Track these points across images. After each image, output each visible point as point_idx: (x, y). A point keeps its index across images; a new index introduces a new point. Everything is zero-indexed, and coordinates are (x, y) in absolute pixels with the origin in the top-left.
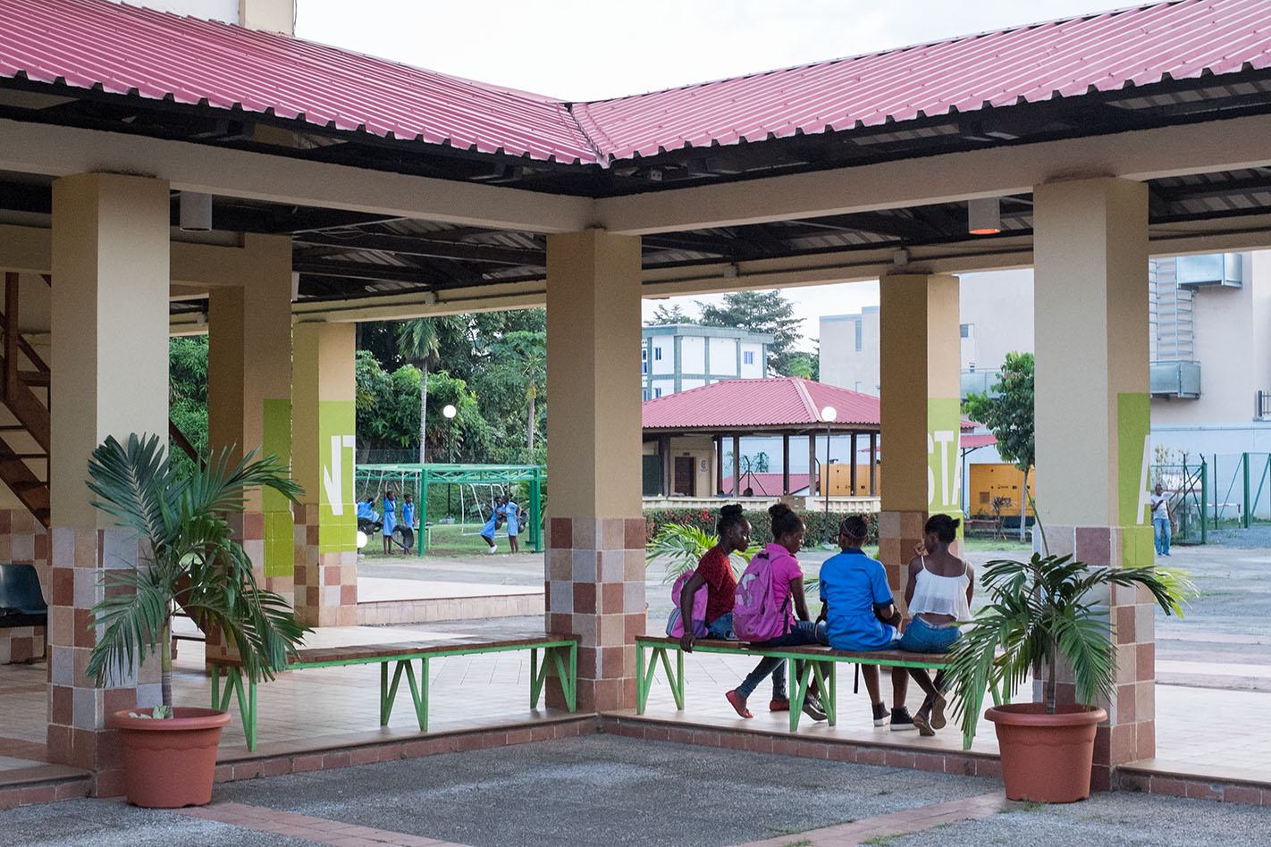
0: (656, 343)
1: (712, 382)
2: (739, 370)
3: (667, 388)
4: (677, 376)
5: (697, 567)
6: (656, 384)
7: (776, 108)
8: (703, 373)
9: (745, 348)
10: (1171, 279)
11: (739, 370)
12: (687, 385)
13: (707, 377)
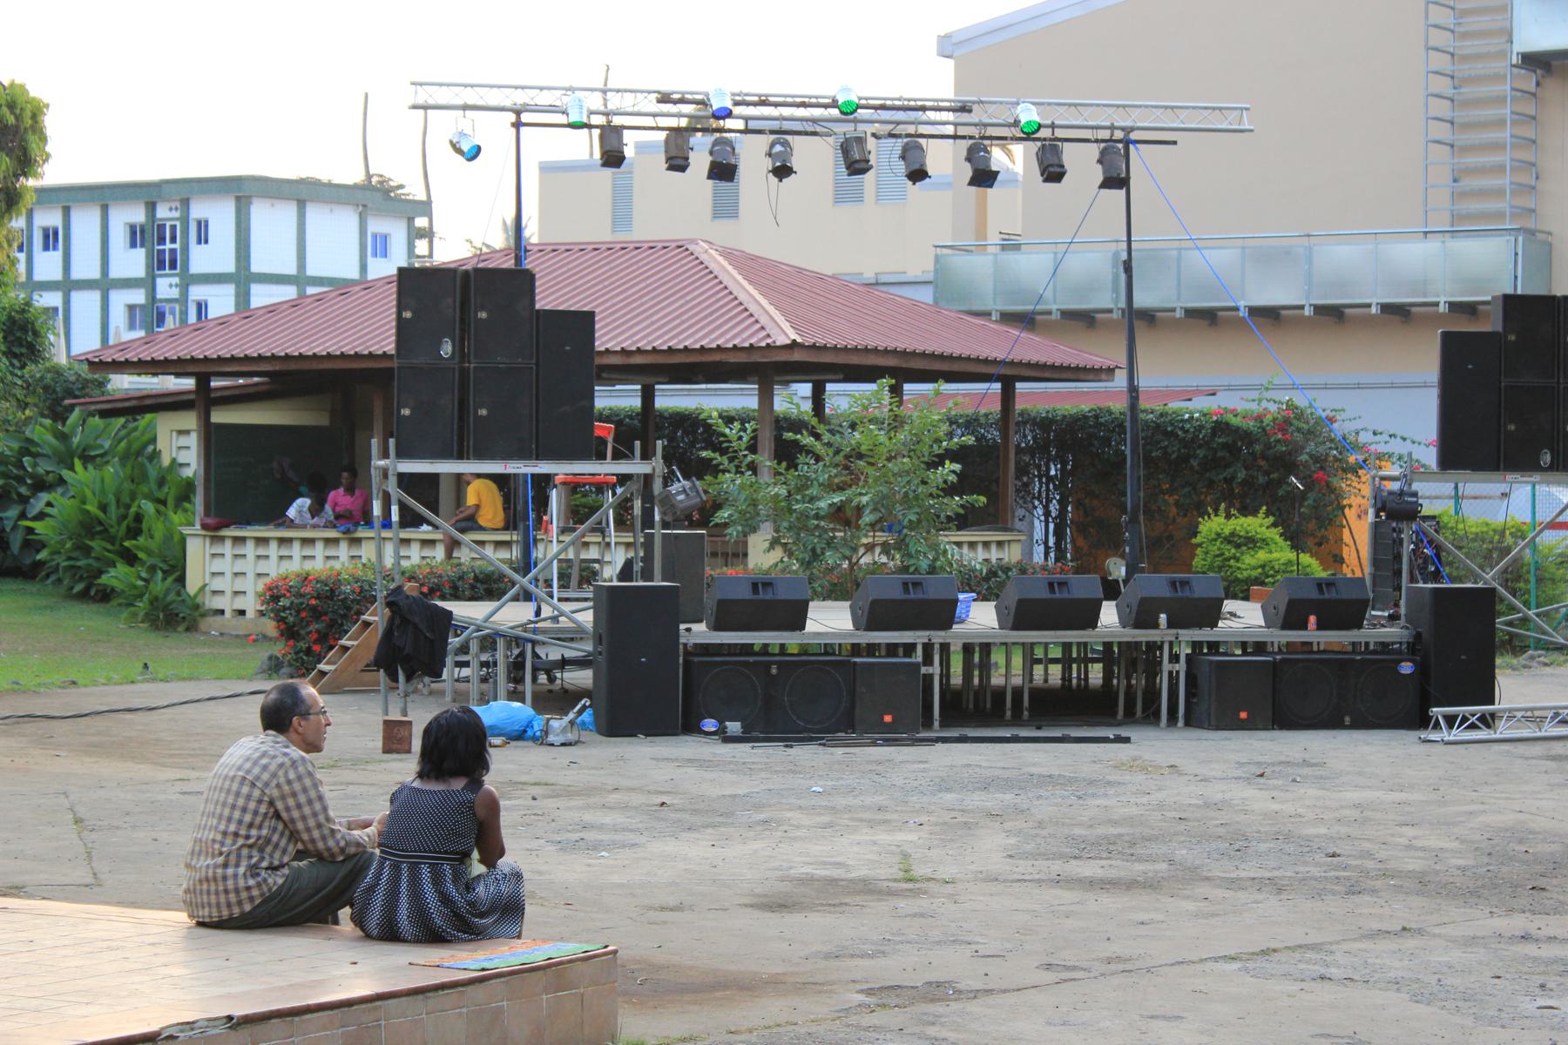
0: (198, 211)
1: (311, 290)
2: (363, 268)
3: (221, 302)
4: (243, 278)
5: (332, 494)
6: (197, 292)
7: (659, 299)
8: (291, 270)
9: (376, 226)
10: (1495, 44)
11: (363, 268)
12: (262, 296)
13: (299, 279)
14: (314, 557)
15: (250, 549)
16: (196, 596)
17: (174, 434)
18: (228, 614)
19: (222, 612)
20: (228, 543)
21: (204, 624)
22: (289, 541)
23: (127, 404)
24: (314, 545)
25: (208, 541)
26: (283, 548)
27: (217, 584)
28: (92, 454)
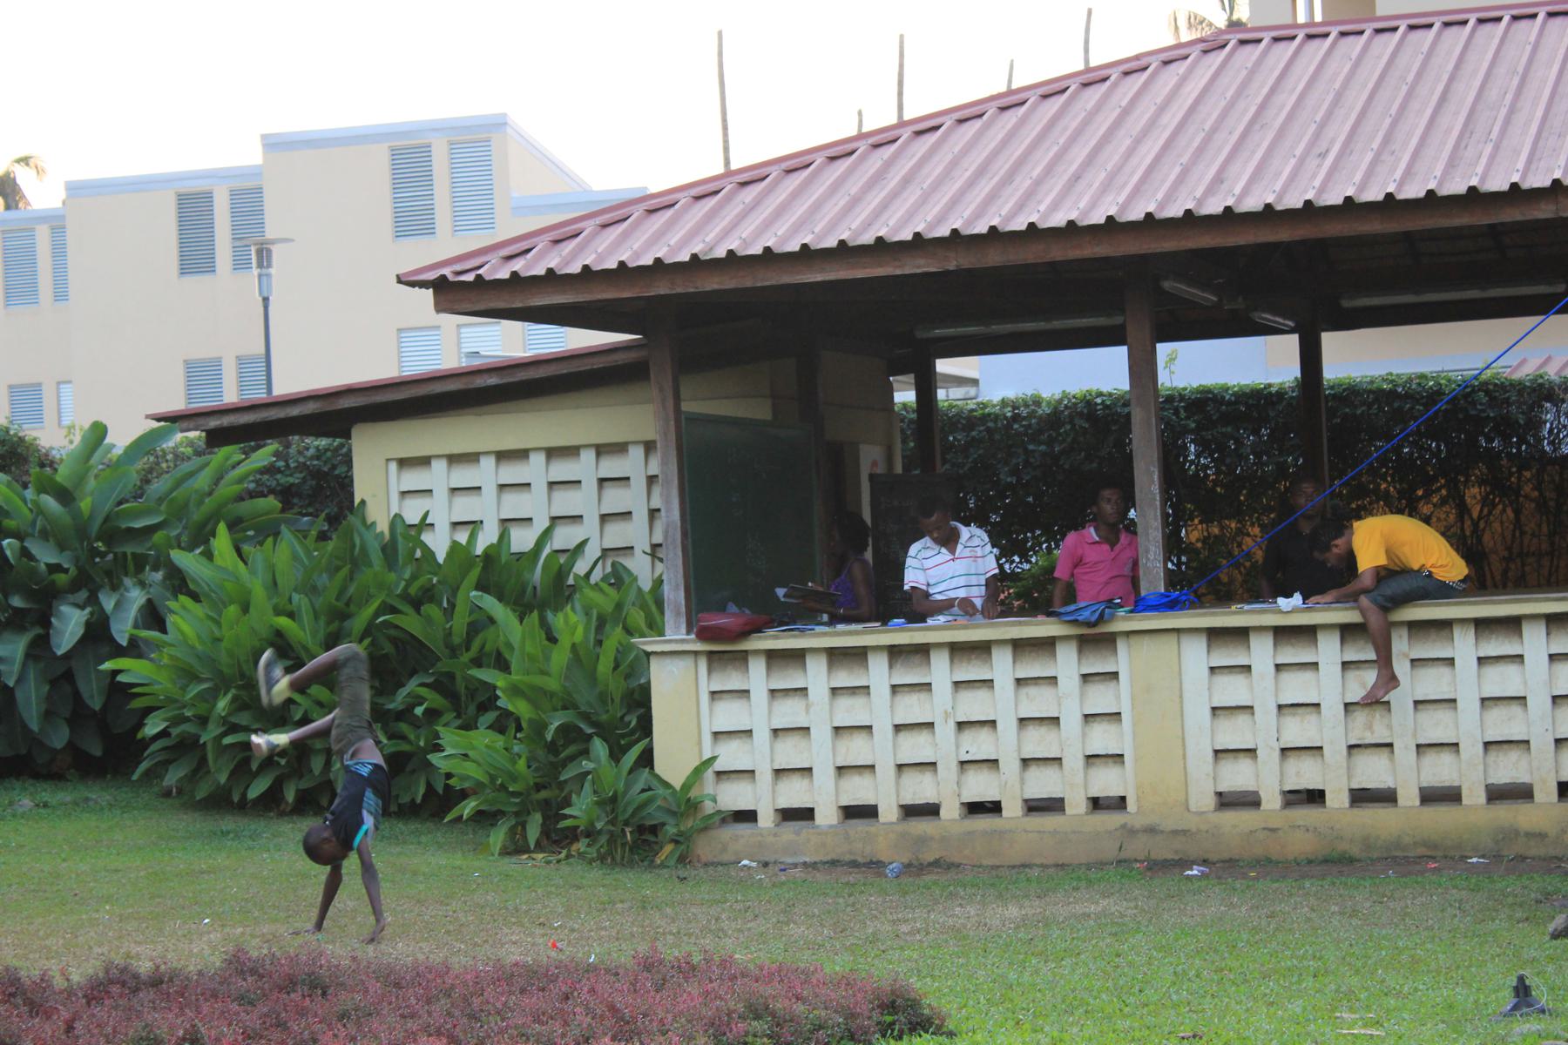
14: (747, 691)
15: (817, 676)
16: (687, 786)
17: (393, 466)
18: (766, 819)
19: (749, 816)
20: (757, 667)
21: (705, 848)
22: (922, 651)
23: (295, 411)
24: (1315, 641)
25: (703, 665)
26: (715, 676)
27: (731, 756)
28: (138, 525)
